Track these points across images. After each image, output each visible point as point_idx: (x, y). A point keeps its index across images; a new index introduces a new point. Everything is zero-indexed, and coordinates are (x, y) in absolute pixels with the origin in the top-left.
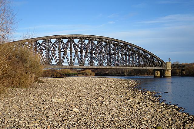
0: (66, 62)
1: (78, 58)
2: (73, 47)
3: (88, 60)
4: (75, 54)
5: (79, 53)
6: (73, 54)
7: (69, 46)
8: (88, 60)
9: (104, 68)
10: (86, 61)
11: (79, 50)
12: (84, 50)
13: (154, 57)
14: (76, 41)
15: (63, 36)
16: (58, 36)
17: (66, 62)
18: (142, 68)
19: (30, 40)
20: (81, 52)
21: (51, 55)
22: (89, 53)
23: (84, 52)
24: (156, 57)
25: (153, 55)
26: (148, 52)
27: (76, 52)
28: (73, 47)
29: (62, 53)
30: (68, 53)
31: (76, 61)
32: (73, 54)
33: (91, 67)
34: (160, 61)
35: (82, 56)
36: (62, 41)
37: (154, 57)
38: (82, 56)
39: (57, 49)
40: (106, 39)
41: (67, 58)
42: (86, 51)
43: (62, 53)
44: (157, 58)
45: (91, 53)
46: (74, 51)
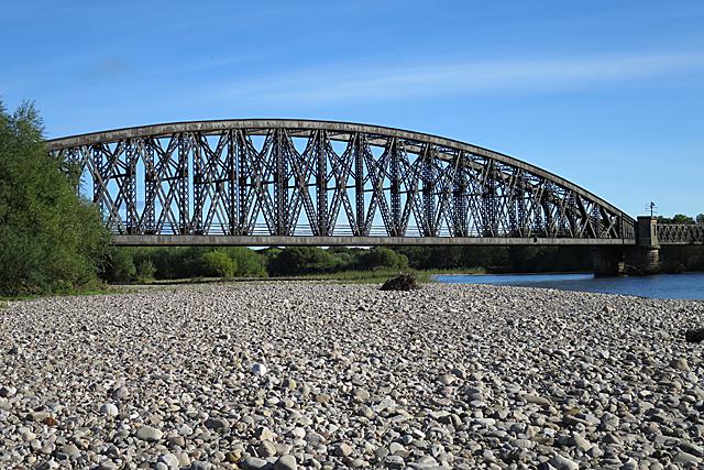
0: (342, 224)
1: (384, 212)
2: (366, 173)
3: (268, 217)
4: (374, 195)
5: (388, 194)
6: (367, 197)
7: (353, 169)
8: (268, 217)
9: (473, 241)
10: (412, 222)
11: (387, 183)
12: (402, 185)
13: (586, 198)
14: (300, 145)
15: (199, 125)
16: (179, 126)
17: (342, 224)
18: (532, 241)
19: (64, 143)
20: (395, 190)
21: (295, 197)
22: (421, 193)
23: (403, 188)
24: (593, 199)
25: (581, 192)
26: (560, 181)
27: (376, 190)
28: (366, 173)
29: (403, 198)
30: (351, 193)
31: (303, 219)
32: (367, 197)
33: (395, 241)
34: (613, 214)
35: (396, 201)
36: (287, 145)
37: (586, 198)
38: (396, 201)
39: (272, 178)
40: (447, 146)
41: (347, 205)
42: (411, 186)
43: (403, 198)
44: (599, 202)
45: (427, 191)
46: (368, 185)
